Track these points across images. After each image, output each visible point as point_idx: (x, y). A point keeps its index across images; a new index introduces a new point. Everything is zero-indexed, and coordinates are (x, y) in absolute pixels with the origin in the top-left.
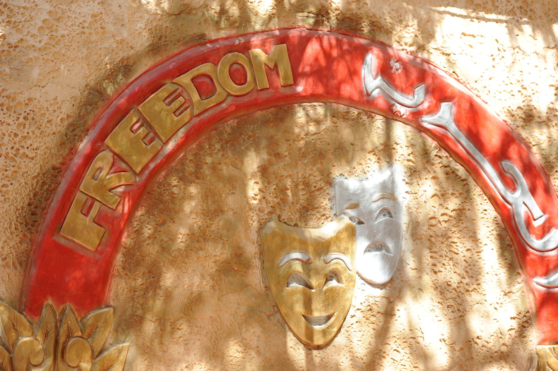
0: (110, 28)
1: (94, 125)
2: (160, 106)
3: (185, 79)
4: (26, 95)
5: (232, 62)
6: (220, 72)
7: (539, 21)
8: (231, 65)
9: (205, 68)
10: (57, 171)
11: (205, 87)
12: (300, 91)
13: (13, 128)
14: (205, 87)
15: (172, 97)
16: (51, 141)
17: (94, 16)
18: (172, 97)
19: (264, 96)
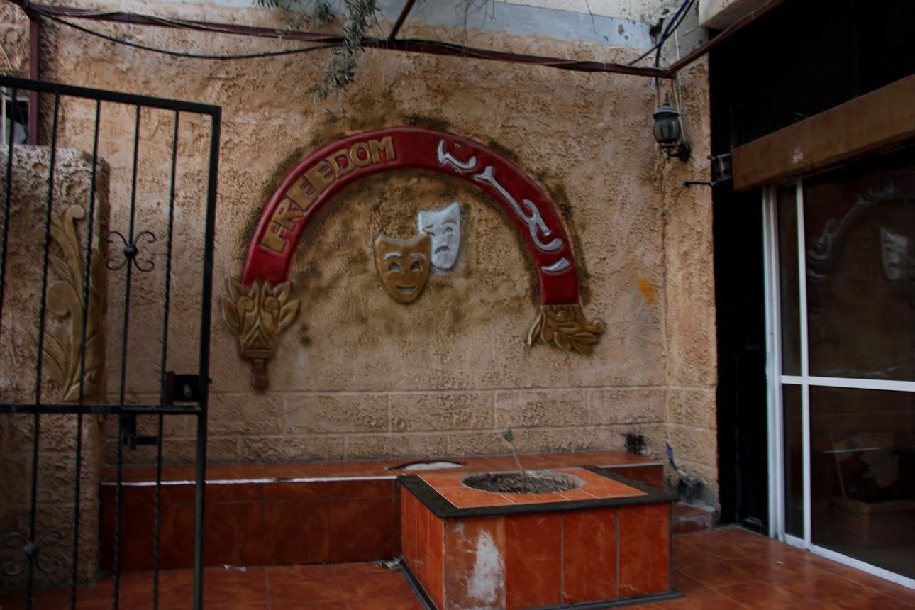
0: (289, 132)
1: (280, 185)
2: (318, 174)
3: (331, 159)
4: (244, 171)
5: (151, 230)
6: (352, 154)
7: (553, 116)
8: (358, 151)
9: (343, 152)
10: (260, 211)
11: (343, 162)
12: (799, 163)
13: (237, 188)
14: (343, 162)
15: (218, 29)
16: (257, 194)
17: (280, 126)
18: (218, 29)
19: (377, 166)
